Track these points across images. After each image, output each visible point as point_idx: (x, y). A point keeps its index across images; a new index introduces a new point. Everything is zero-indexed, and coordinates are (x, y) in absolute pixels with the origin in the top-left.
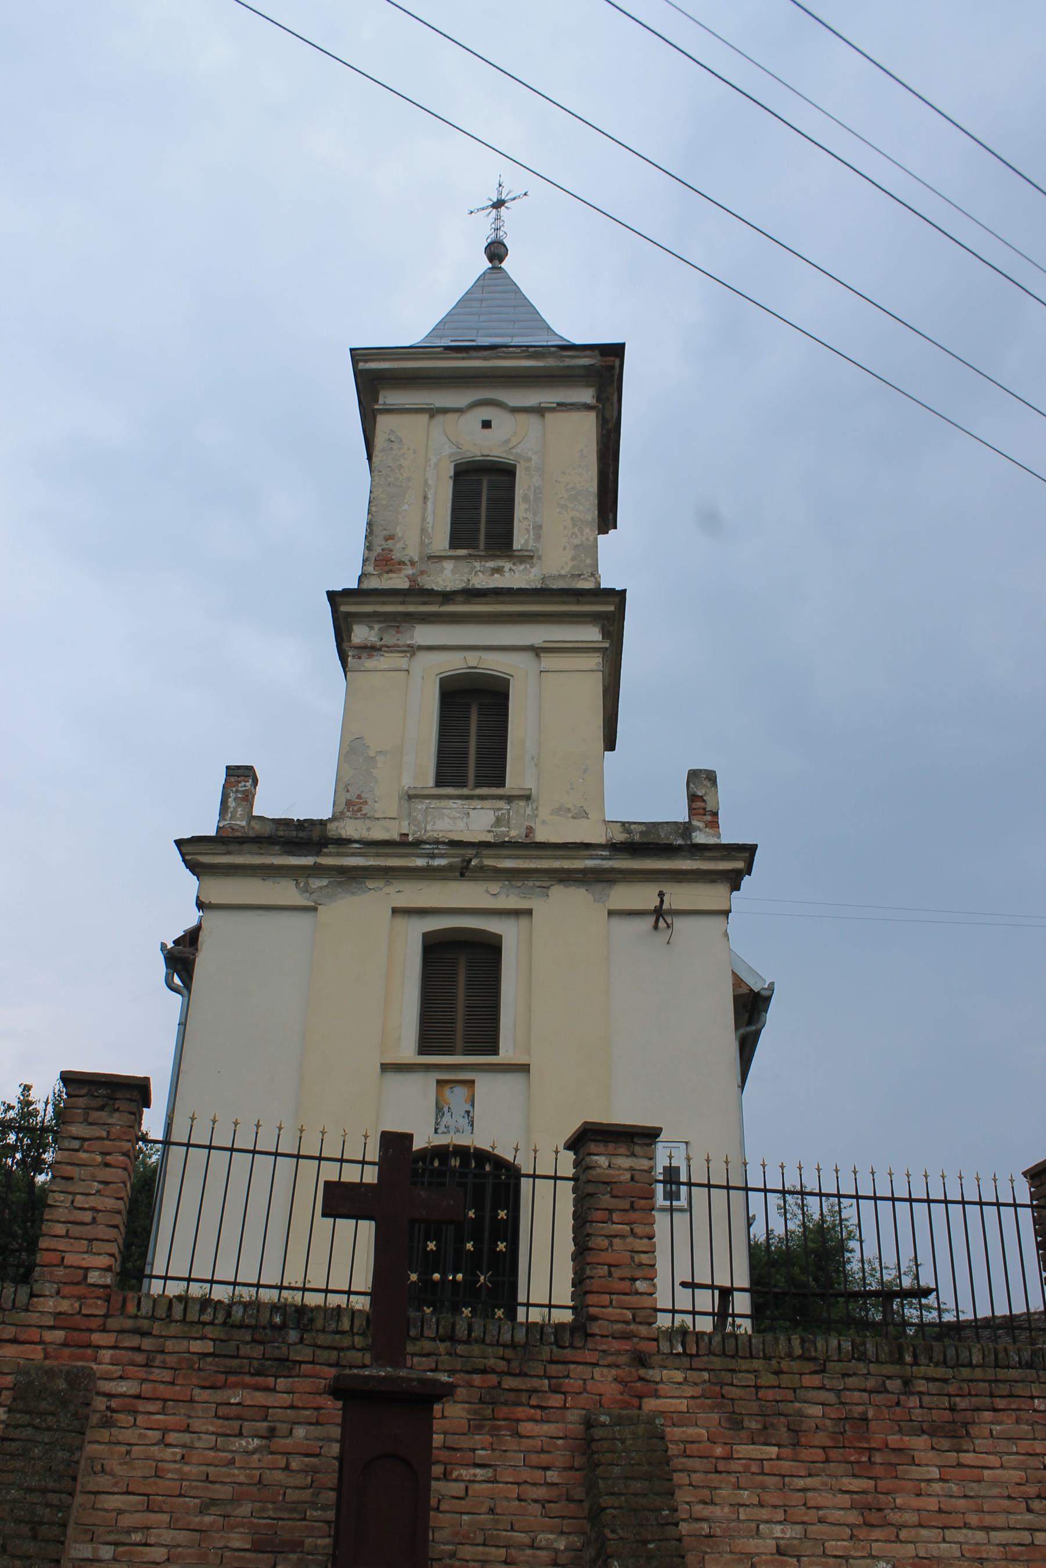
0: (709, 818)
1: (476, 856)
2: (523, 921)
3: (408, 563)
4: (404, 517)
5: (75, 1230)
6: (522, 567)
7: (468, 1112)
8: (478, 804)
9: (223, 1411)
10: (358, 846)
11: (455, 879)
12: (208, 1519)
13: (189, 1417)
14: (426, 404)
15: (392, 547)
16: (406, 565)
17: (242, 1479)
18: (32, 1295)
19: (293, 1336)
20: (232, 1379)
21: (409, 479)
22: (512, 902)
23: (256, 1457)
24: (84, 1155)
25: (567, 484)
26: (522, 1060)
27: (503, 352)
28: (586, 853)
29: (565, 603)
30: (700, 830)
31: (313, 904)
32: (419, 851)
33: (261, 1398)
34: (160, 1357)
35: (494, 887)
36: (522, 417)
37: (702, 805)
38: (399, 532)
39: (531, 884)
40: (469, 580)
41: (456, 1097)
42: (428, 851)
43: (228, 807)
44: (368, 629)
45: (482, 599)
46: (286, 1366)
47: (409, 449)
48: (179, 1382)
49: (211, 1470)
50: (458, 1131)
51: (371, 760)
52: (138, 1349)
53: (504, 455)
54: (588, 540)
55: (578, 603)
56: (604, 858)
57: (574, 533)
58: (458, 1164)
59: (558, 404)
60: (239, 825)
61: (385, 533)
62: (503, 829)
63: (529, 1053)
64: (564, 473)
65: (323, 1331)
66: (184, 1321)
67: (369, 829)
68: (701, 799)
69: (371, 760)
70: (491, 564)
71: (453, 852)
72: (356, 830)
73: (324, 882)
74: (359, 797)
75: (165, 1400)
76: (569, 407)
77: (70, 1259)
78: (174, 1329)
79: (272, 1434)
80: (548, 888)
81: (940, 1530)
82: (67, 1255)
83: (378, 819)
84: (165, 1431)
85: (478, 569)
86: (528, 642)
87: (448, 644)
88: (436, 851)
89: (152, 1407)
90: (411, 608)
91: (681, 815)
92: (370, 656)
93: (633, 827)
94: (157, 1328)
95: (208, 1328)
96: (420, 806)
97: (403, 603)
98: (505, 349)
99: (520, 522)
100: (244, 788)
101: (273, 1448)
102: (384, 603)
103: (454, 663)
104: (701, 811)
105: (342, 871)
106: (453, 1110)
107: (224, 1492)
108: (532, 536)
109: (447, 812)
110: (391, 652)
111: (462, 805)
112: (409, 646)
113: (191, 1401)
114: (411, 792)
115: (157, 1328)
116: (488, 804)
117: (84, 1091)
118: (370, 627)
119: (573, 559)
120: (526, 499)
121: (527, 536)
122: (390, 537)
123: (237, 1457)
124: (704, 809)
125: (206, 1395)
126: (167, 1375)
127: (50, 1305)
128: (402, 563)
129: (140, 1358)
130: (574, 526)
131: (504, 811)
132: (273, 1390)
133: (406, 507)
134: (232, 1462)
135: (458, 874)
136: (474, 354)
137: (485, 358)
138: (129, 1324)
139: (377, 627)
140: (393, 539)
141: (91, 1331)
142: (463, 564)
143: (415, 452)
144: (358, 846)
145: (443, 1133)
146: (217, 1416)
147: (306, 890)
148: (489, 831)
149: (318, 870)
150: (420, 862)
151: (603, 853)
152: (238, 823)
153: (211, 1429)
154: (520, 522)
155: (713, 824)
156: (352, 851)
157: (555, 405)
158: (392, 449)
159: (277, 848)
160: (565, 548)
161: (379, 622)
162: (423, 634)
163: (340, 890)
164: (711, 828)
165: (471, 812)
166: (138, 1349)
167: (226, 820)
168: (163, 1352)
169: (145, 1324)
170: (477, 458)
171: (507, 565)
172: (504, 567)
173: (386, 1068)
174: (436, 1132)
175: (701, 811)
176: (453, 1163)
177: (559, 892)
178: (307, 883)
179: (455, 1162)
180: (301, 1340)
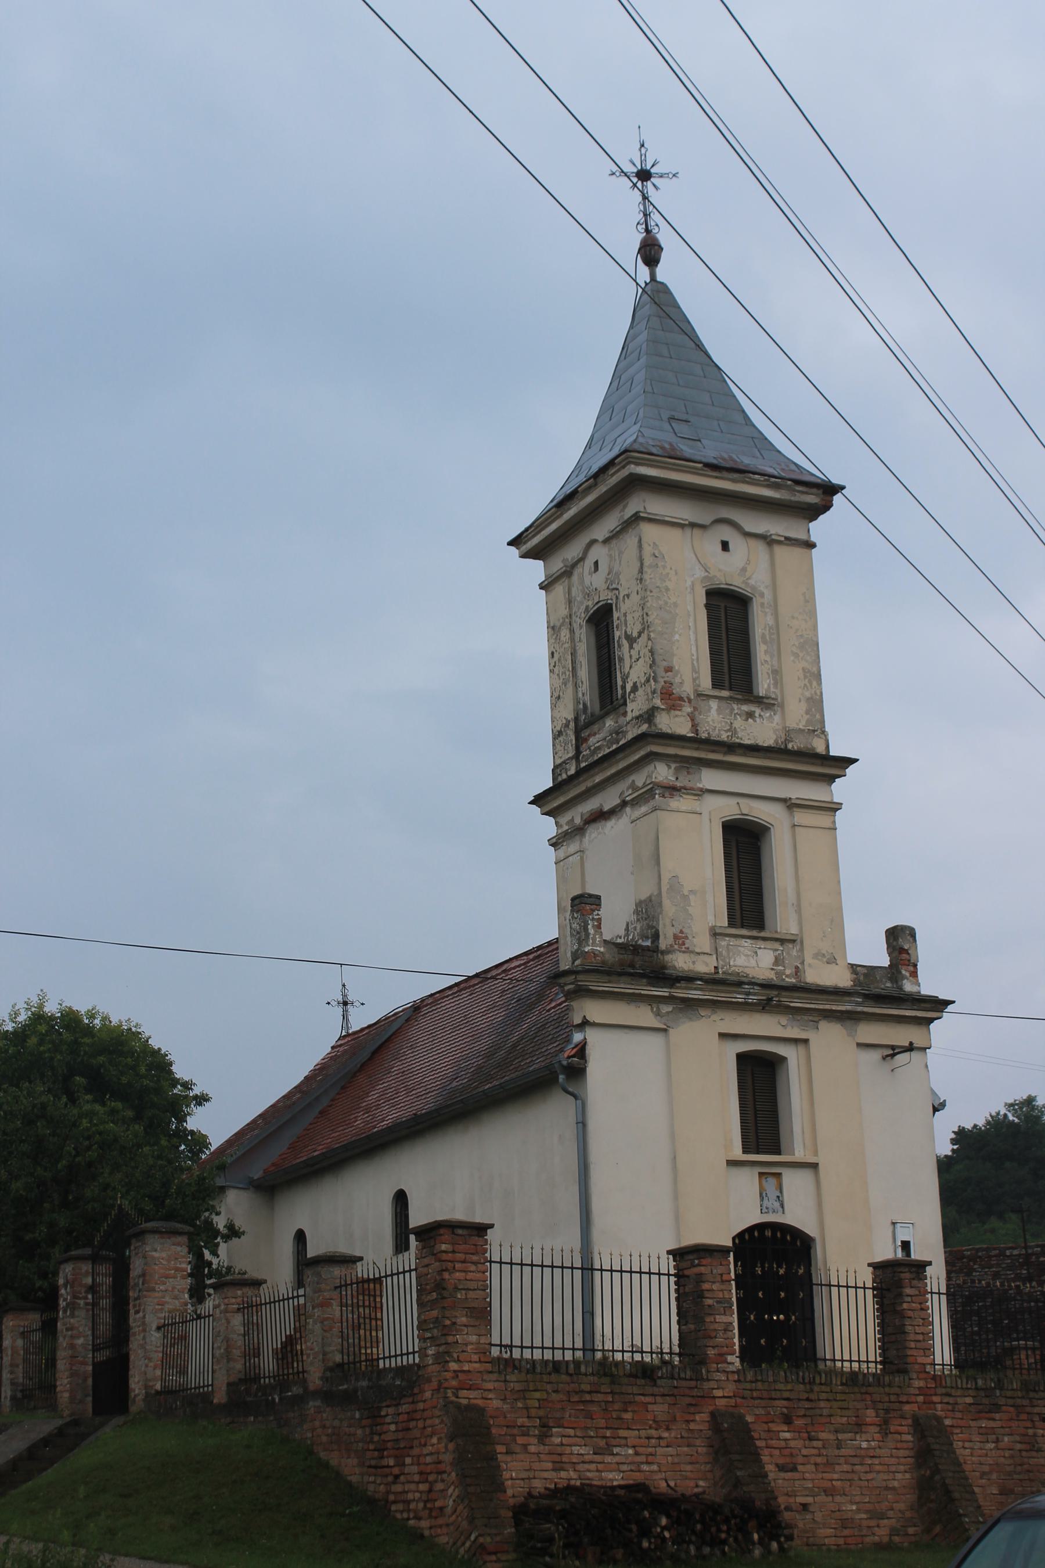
0: (911, 968)
1: (776, 996)
2: (801, 1048)
3: (686, 700)
4: (678, 648)
5: (919, 1345)
6: (768, 715)
7: (778, 1197)
8: (761, 944)
9: (981, 1431)
10: (700, 983)
11: (758, 1011)
12: (984, 1481)
13: (970, 1434)
14: (682, 519)
15: (673, 680)
16: (685, 702)
17: (991, 1462)
18: (910, 1379)
19: (998, 1393)
20: (981, 1415)
21: (675, 605)
22: (794, 1032)
23: (993, 1452)
24: (914, 1305)
25: (797, 630)
26: (812, 1160)
27: (750, 478)
28: (848, 999)
29: (813, 764)
30: (908, 979)
31: (665, 1027)
32: (740, 990)
33: (991, 1424)
34: (956, 1406)
35: (784, 1020)
36: (753, 543)
37: (907, 956)
38: (676, 663)
39: (806, 1018)
40: (731, 723)
41: (771, 1184)
42: (746, 990)
43: (589, 934)
44: (666, 768)
45: (756, 754)
46: (996, 1408)
47: (671, 569)
48: (965, 1418)
49: (981, 1459)
50: (774, 1211)
51: (685, 898)
52: (947, 1403)
53: (743, 586)
54: (816, 693)
55: (822, 765)
56: (858, 1004)
57: (805, 685)
58: (770, 1234)
59: (787, 538)
60: (599, 951)
61: (665, 664)
62: (781, 968)
63: (816, 1153)
64: (793, 617)
65: (1007, 1390)
66: (962, 1388)
67: (694, 963)
68: (907, 952)
69: (685, 898)
70: (745, 708)
71: (763, 992)
72: (685, 963)
73: (670, 1008)
74: (681, 932)
75: (961, 1427)
76: (793, 542)
77: (920, 1360)
78: (959, 1392)
79: (997, 1441)
80: (817, 1022)
81: (581, 1439)
82: (918, 1358)
83: (699, 954)
84: (964, 1441)
85: (736, 711)
86: (783, 796)
87: (727, 790)
88: (751, 991)
89: (957, 1431)
90: (703, 755)
91: (884, 961)
92: (672, 796)
93: (858, 968)
94: (953, 1392)
95: (970, 1391)
96: (723, 943)
97: (697, 749)
98: (751, 475)
99: (762, 664)
100: (597, 917)
101: (999, 1447)
102: (683, 747)
103: (729, 809)
104: (907, 963)
105: (684, 1000)
106: (768, 1195)
107: (986, 1469)
108: (772, 682)
109: (742, 949)
110: (687, 794)
111: (751, 944)
112: (701, 790)
113: (970, 1427)
114: (718, 931)
115: (953, 1392)
116: (769, 944)
117: (907, 1270)
118: (668, 765)
119: (807, 712)
120: (765, 642)
121: (768, 681)
122: (669, 669)
123: (989, 1452)
124: (909, 960)
125: (972, 1424)
126: (959, 1415)
127: (917, 1383)
128: (681, 699)
129: (950, 1407)
130: (805, 677)
131: (779, 952)
132: (994, 1420)
133: (677, 637)
134: (986, 1455)
135: (761, 1008)
136: (725, 474)
137: (734, 481)
138: (944, 1391)
139: (673, 766)
140: (671, 671)
141: (931, 1395)
142: (724, 704)
143: (676, 571)
144: (700, 983)
145: (766, 1213)
146: (979, 1434)
147: (658, 1014)
148: (772, 969)
149: (670, 999)
150: (740, 998)
151: (858, 1000)
152: (598, 948)
153: (978, 1440)
154: (762, 664)
155: (914, 974)
156: (695, 986)
157: (783, 539)
158: (657, 566)
159: (645, 980)
160: (800, 701)
161: (675, 762)
162: (710, 779)
163: (681, 1015)
164: (913, 977)
165: (759, 952)
166: (947, 1403)
167: (589, 946)
168: (956, 1404)
169: (949, 1390)
170: (722, 586)
171: (758, 712)
172: (754, 712)
173: (732, 1163)
174: (762, 1213)
175: (907, 963)
176: (766, 1234)
177: (823, 1025)
178: (658, 1008)
179: (768, 1233)
180: (1001, 1395)
